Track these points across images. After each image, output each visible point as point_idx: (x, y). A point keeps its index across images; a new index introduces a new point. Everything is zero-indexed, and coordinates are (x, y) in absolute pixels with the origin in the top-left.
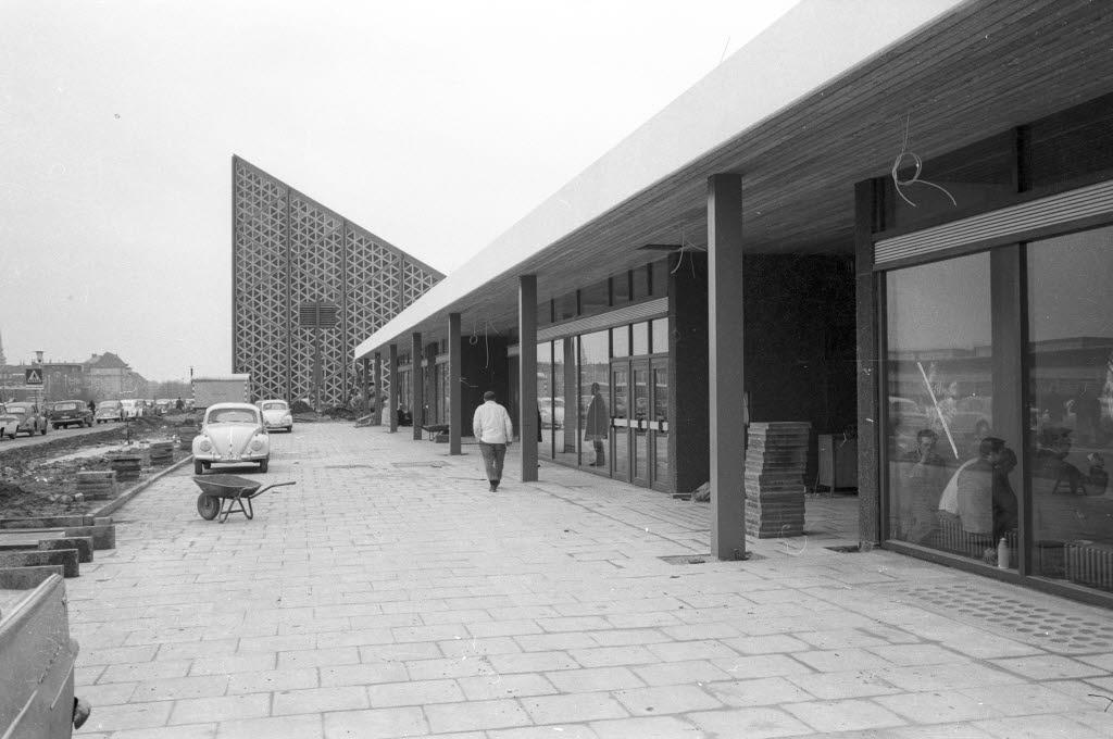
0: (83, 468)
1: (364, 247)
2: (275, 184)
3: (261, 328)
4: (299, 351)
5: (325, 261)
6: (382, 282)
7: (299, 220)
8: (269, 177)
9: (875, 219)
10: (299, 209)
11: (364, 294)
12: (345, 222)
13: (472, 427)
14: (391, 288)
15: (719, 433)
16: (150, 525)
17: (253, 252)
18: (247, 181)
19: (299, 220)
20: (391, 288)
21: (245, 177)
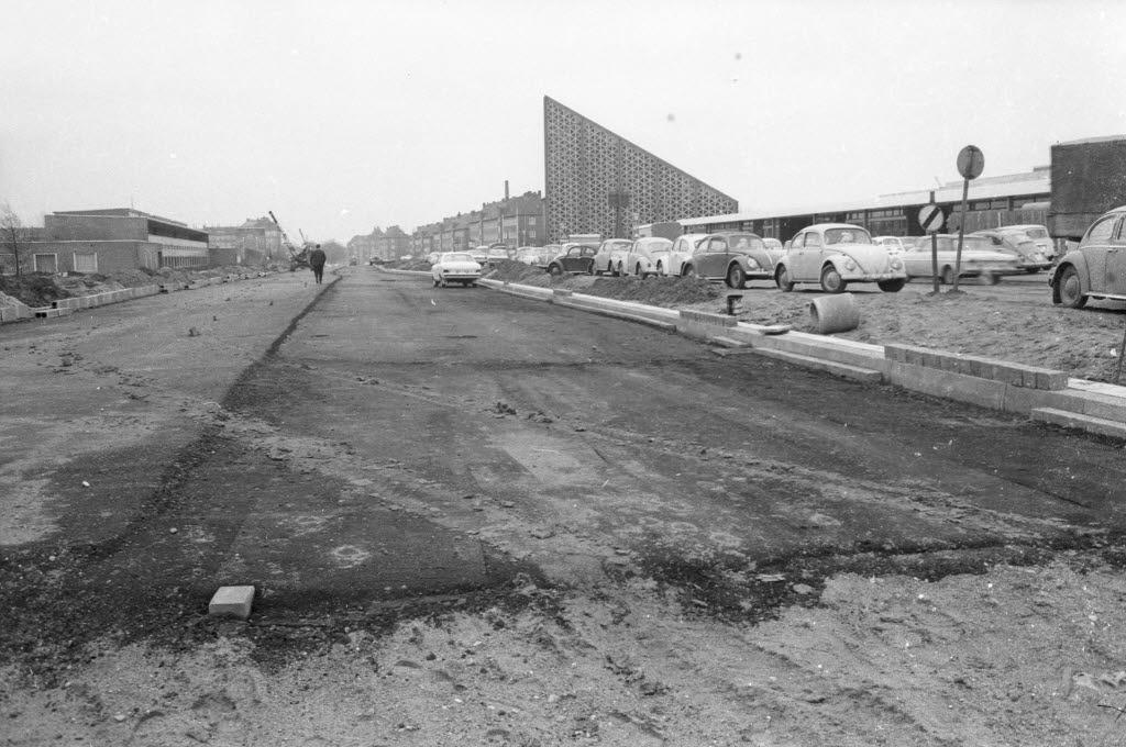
0: (448, 365)
1: (632, 154)
2: (573, 114)
3: (566, 205)
4: (590, 220)
5: (607, 163)
6: (644, 177)
7: (589, 138)
8: (599, 127)
9: (959, 545)
10: (589, 130)
11: (632, 184)
12: (620, 139)
13: (805, 226)
14: (650, 180)
15: (607, 296)
16: (94, 658)
17: (559, 158)
18: (554, 112)
19: (589, 138)
20: (650, 180)
21: (554, 112)
